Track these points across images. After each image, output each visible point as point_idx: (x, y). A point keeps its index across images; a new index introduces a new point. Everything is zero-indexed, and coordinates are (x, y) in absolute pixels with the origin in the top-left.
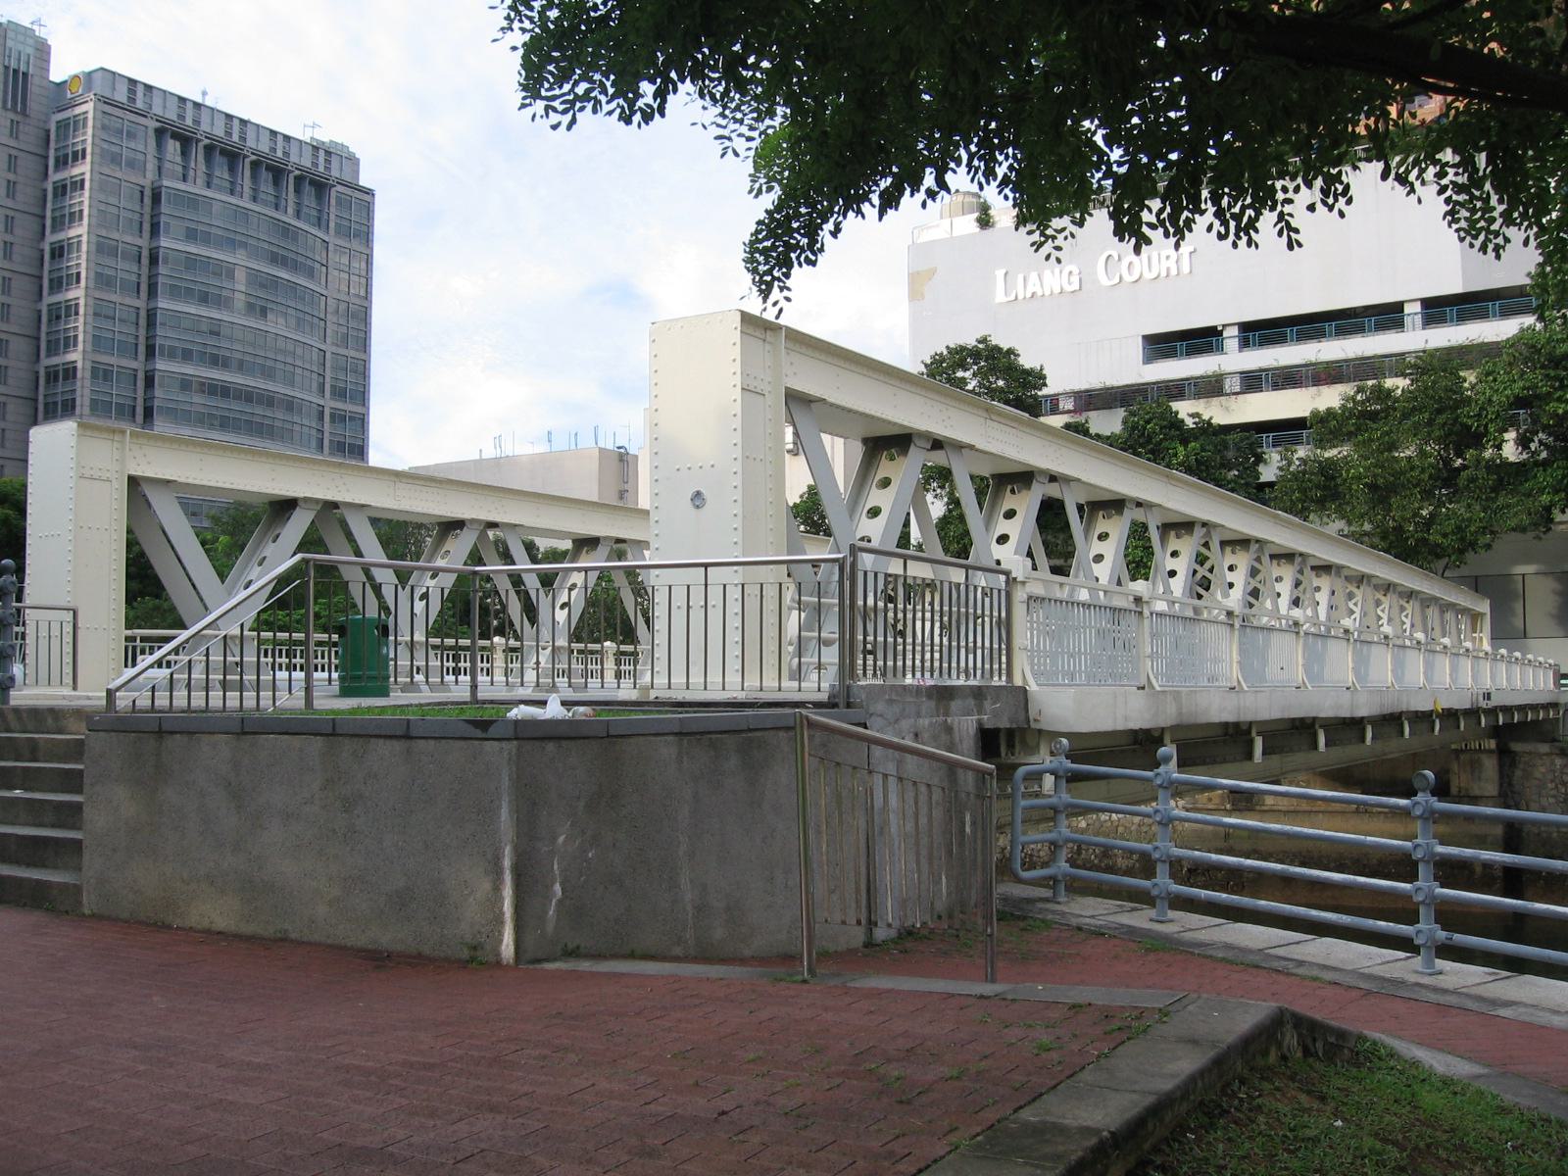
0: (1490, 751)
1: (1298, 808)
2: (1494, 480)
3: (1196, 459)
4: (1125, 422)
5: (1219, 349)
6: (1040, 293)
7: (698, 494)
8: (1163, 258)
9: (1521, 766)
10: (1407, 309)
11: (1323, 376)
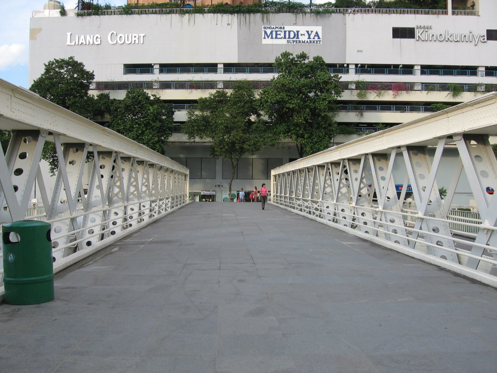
3: (157, 112)
4: (127, 95)
8: (133, 37)
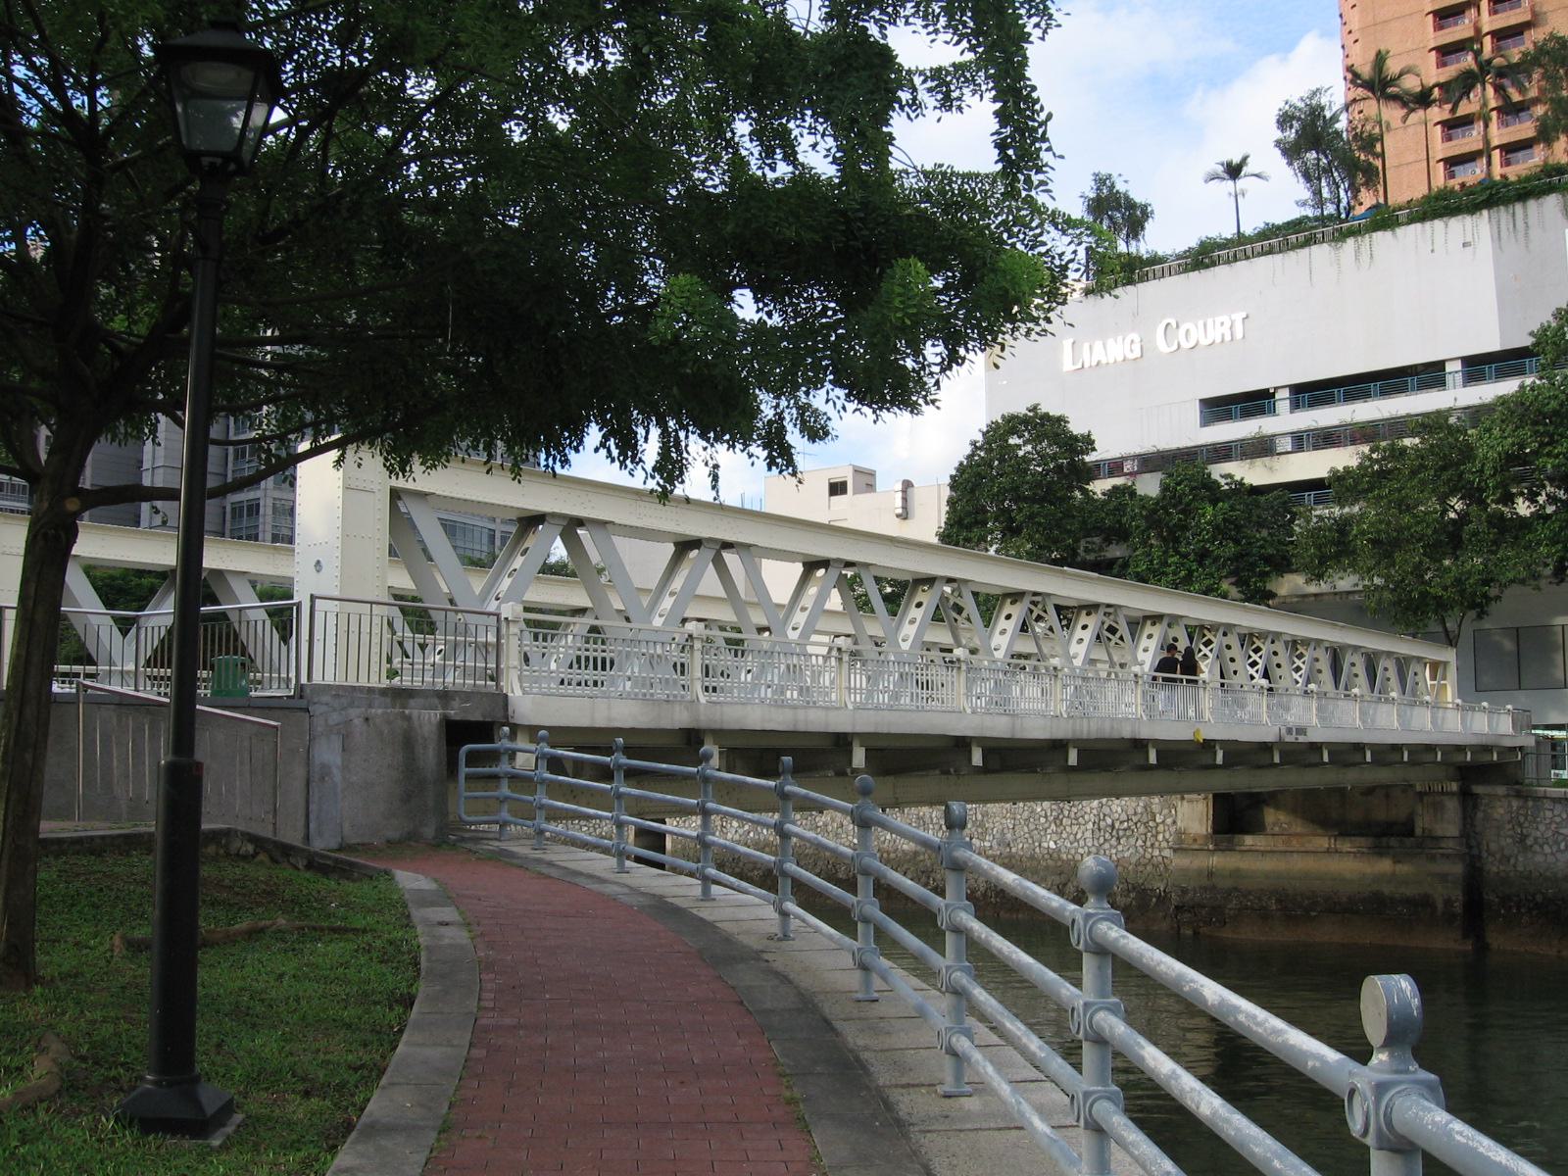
0: (1452, 794)
1: (1275, 849)
2: (1495, 534)
5: (1272, 411)
6: (1104, 361)
7: (318, 562)
8: (1218, 324)
9: (1482, 808)
10: (1449, 367)
11: (1358, 436)
